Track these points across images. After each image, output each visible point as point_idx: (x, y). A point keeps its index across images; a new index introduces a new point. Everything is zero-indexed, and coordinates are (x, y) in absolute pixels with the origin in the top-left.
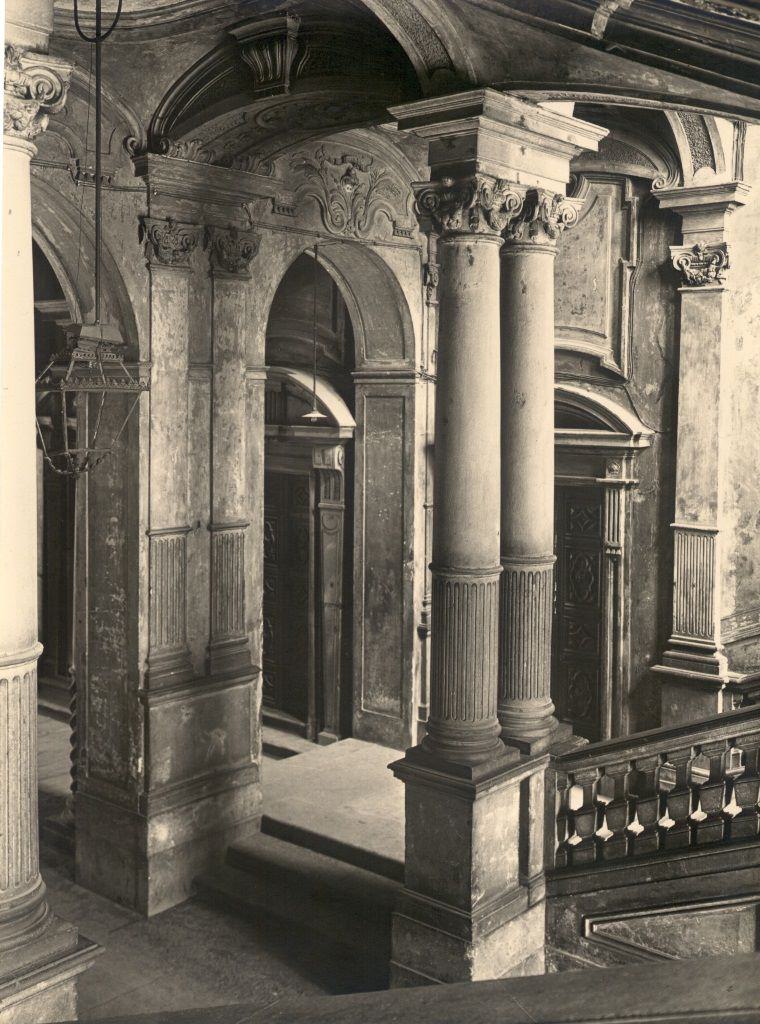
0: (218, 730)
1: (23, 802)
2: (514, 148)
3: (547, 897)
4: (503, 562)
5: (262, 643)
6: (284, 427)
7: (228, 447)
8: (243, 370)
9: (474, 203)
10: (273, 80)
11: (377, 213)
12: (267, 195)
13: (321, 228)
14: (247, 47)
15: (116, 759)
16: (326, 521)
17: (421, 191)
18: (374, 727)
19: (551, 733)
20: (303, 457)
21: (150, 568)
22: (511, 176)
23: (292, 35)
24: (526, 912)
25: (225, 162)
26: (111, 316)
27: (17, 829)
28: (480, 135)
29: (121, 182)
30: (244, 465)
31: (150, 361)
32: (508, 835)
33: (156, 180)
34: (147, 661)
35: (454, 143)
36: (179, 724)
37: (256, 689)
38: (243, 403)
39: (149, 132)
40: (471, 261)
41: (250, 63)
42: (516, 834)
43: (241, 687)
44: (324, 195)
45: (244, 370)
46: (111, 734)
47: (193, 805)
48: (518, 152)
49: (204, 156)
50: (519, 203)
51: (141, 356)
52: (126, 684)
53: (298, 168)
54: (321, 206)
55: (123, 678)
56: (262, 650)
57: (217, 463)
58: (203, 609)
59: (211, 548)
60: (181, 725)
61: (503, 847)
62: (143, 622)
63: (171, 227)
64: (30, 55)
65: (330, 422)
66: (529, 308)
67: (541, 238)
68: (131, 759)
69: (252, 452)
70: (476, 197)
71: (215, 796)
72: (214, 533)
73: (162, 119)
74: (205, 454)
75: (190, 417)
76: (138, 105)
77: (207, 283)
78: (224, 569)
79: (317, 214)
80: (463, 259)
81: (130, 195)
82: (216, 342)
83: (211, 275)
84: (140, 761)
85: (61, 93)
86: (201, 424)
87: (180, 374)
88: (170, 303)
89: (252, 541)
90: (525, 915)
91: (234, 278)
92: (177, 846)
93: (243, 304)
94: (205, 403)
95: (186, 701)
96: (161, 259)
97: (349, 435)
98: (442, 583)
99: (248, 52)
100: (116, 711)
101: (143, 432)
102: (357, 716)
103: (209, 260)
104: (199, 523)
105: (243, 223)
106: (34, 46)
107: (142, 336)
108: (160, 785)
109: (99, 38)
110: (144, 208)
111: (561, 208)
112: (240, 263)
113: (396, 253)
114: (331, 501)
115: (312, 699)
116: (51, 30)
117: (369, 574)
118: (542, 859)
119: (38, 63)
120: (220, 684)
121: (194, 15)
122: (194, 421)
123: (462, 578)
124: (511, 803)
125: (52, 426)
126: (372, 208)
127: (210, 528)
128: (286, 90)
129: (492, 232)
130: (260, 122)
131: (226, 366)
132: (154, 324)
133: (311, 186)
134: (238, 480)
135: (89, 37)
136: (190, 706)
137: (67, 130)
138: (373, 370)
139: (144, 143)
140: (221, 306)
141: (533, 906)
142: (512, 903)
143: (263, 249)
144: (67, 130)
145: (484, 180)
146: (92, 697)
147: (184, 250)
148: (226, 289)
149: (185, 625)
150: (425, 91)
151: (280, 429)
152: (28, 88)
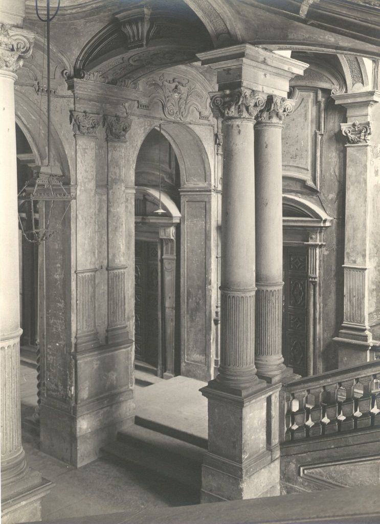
0: (112, 372)
2: (261, 74)
3: (281, 456)
4: (257, 285)
5: (134, 327)
6: (145, 217)
8: (123, 188)
9: (240, 102)
11: (191, 108)
13: (163, 116)
14: (124, 24)
15: (61, 388)
16: (167, 265)
17: (213, 97)
18: (192, 370)
19: (282, 372)
21: (77, 290)
22: (260, 88)
23: (147, 17)
24: (270, 464)
25: (113, 82)
26: (56, 161)
27: (10, 423)
30: (124, 237)
31: (76, 184)
33: (79, 91)
34: (76, 337)
36: (93, 369)
37: (131, 351)
38: (124, 205)
39: (75, 67)
40: (239, 132)
41: (126, 32)
43: (124, 350)
44: (164, 98)
47: (100, 411)
48: (263, 77)
49: (103, 79)
50: (263, 102)
51: (71, 182)
52: (65, 349)
53: (151, 85)
56: (134, 331)
57: (110, 236)
58: (104, 310)
62: (73, 317)
63: (86, 116)
64: (13, 28)
65: (168, 215)
67: (275, 120)
68: (68, 387)
70: (241, 99)
71: (111, 406)
73: (81, 61)
74: (105, 232)
75: (97, 212)
76: (69, 54)
77: (105, 144)
78: (115, 290)
79: (161, 108)
80: (235, 131)
81: (65, 100)
82: (110, 174)
83: (107, 140)
84: (73, 388)
86: (102, 217)
89: (129, 275)
90: (270, 466)
91: (119, 141)
92: (92, 431)
93: (123, 155)
94: (104, 205)
95: (96, 358)
96: (81, 133)
97: (178, 221)
98: (226, 296)
99: (125, 27)
100: (60, 363)
102: (183, 364)
104: (102, 266)
105: (123, 113)
106: (16, 24)
107: (72, 172)
108: (83, 400)
110: (72, 106)
115: (159, 351)
117: (189, 293)
118: (278, 437)
119: (17, 33)
120: (113, 348)
122: (98, 215)
125: (26, 218)
126: (189, 105)
127: (107, 269)
128: (145, 46)
130: (131, 62)
131: (114, 186)
133: (157, 95)
134: (122, 245)
136: (98, 360)
137: (33, 67)
139: (72, 73)
141: (274, 461)
142: (262, 459)
143: (133, 126)
146: (48, 356)
147: (93, 127)
148: (115, 147)
149: (95, 318)
150: (215, 47)
151: (143, 219)
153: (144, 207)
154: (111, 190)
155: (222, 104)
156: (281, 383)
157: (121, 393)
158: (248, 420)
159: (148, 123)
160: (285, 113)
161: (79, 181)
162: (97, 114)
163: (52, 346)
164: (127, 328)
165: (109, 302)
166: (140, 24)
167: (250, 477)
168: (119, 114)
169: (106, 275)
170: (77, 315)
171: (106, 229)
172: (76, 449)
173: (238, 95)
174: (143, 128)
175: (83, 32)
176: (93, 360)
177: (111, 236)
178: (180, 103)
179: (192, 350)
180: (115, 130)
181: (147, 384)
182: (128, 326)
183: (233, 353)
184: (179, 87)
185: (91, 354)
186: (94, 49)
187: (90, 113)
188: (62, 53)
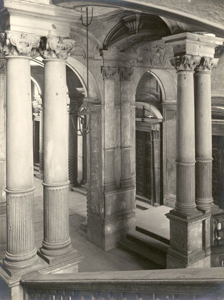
0: (123, 202)
1: (65, 219)
3: (211, 254)
4: (196, 159)
7: (125, 126)
8: (129, 105)
9: (185, 63)
10: (133, 31)
11: (167, 61)
12: (135, 58)
13: (151, 66)
14: (127, 22)
15: (97, 209)
16: (155, 145)
17: (171, 60)
18: (169, 203)
20: (149, 127)
21: (105, 158)
23: (138, 19)
24: (204, 258)
25: (123, 51)
27: (63, 226)
28: (187, 44)
29: (96, 58)
30: (130, 131)
32: (199, 235)
33: (105, 57)
34: (104, 183)
35: (180, 46)
38: (129, 115)
39: (103, 44)
41: (128, 26)
42: (201, 235)
43: (130, 190)
45: (130, 105)
46: (96, 202)
48: (198, 48)
50: (199, 61)
52: (99, 189)
53: (144, 50)
54: (151, 60)
55: (98, 187)
57: (122, 131)
58: (119, 169)
59: (121, 153)
60: (114, 200)
61: (197, 239)
62: (103, 173)
63: (109, 69)
64: (65, 39)
65: (155, 118)
66: (203, 89)
67: (206, 70)
68: (101, 209)
69: (132, 127)
70: (185, 61)
71: (123, 220)
72: (122, 149)
73: (106, 41)
75: (115, 118)
77: (119, 83)
80: (183, 77)
81: (99, 61)
82: (122, 98)
83: (120, 80)
84: (103, 209)
85: (72, 47)
87: (112, 107)
88: (109, 89)
91: (126, 81)
93: (129, 88)
94: (119, 114)
97: (161, 121)
99: (127, 23)
101: (103, 122)
102: (164, 199)
103: (120, 76)
106: (66, 37)
107: (102, 98)
108: (108, 216)
109: (87, 25)
110: (102, 64)
111: (212, 61)
112: (128, 77)
113: (172, 71)
114: (157, 139)
115: (150, 191)
116: (70, 32)
117: (167, 160)
119: (67, 41)
120: (124, 190)
121: (113, 15)
122: (116, 119)
123: (184, 164)
124: (199, 227)
127: (121, 148)
128: (137, 33)
129: (191, 70)
131: (124, 104)
132: (105, 94)
135: (85, 25)
136: (116, 195)
138: (168, 103)
139: (102, 47)
140: (123, 88)
142: (199, 256)
143: (135, 72)
144: (83, 46)
145: (188, 56)
146: (91, 192)
147: (113, 75)
148: (125, 84)
149: (114, 173)
150: (172, 33)
152: (65, 47)
153: (141, 114)
154: (123, 107)
155: (176, 63)
156: (211, 214)
157: (128, 213)
158: (191, 233)
159: (142, 70)
160: (213, 66)
161: (106, 102)
162: (115, 67)
163: (93, 187)
164: (131, 179)
165: (122, 165)
166: (134, 22)
167: (192, 264)
168: (127, 66)
169: (120, 150)
170: (105, 171)
171: (120, 127)
172: (105, 242)
173: (184, 59)
174: (140, 73)
175: (107, 27)
176: (113, 195)
177: (123, 130)
178: (160, 58)
179: (169, 192)
180: (125, 75)
181: (145, 209)
182: (132, 178)
183: (182, 196)
184: (159, 50)
185: (112, 192)
186: (114, 34)
187: (111, 67)
188: (97, 37)
